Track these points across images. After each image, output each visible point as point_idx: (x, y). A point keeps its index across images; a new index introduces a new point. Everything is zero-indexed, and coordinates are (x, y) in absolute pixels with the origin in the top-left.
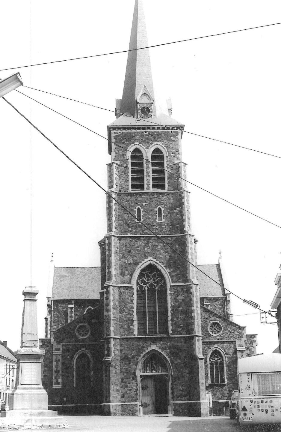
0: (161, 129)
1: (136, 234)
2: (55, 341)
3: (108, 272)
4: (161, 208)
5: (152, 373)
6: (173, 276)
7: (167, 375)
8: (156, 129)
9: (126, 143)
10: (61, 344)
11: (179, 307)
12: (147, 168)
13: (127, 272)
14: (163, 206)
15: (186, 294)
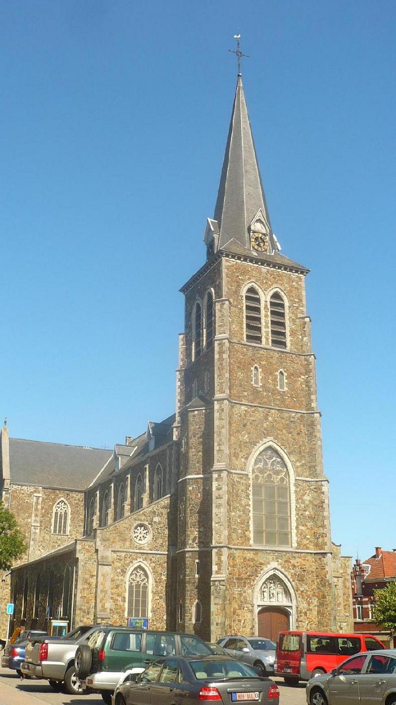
0: (294, 271)
4: (283, 372)
5: (270, 603)
6: (298, 467)
8: (230, 257)
10: (110, 549)
12: (265, 317)
14: (286, 370)
15: (315, 494)
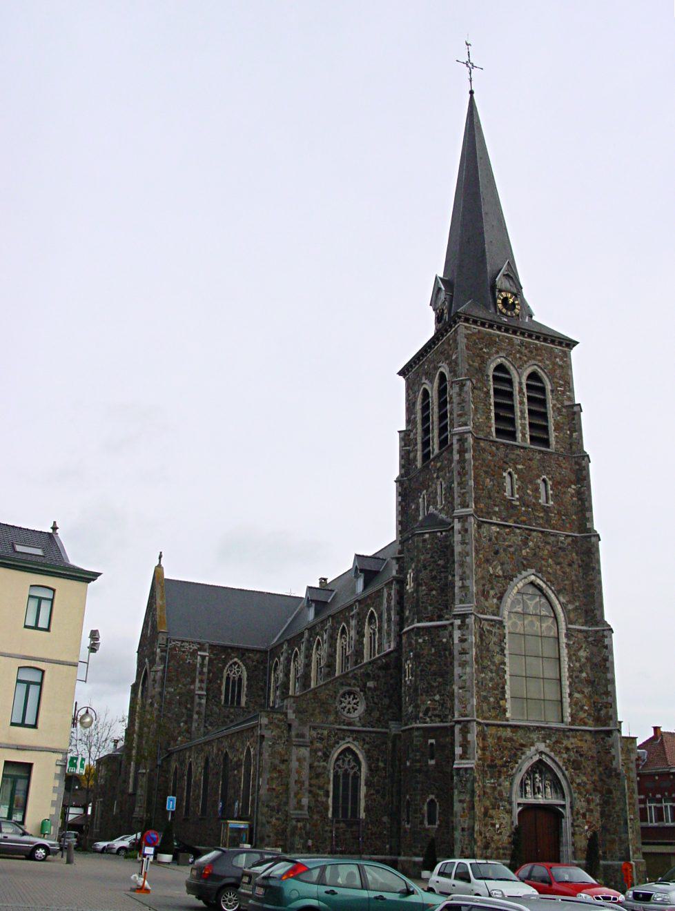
1: (506, 521)
2: (296, 717)
3: (460, 588)
4: (547, 479)
7: (563, 806)
9: (484, 350)
11: (581, 672)
12: (520, 404)
13: (492, 593)
